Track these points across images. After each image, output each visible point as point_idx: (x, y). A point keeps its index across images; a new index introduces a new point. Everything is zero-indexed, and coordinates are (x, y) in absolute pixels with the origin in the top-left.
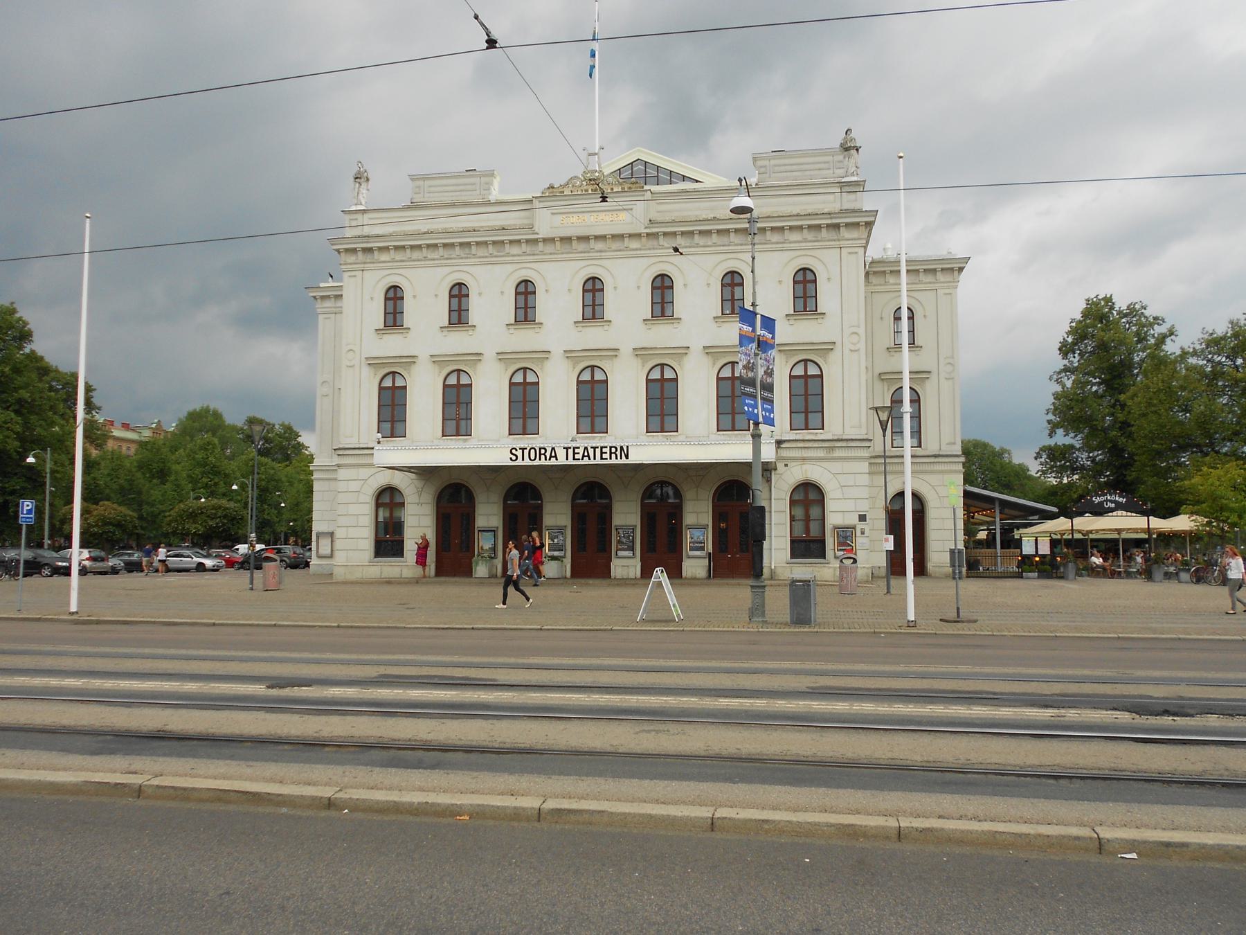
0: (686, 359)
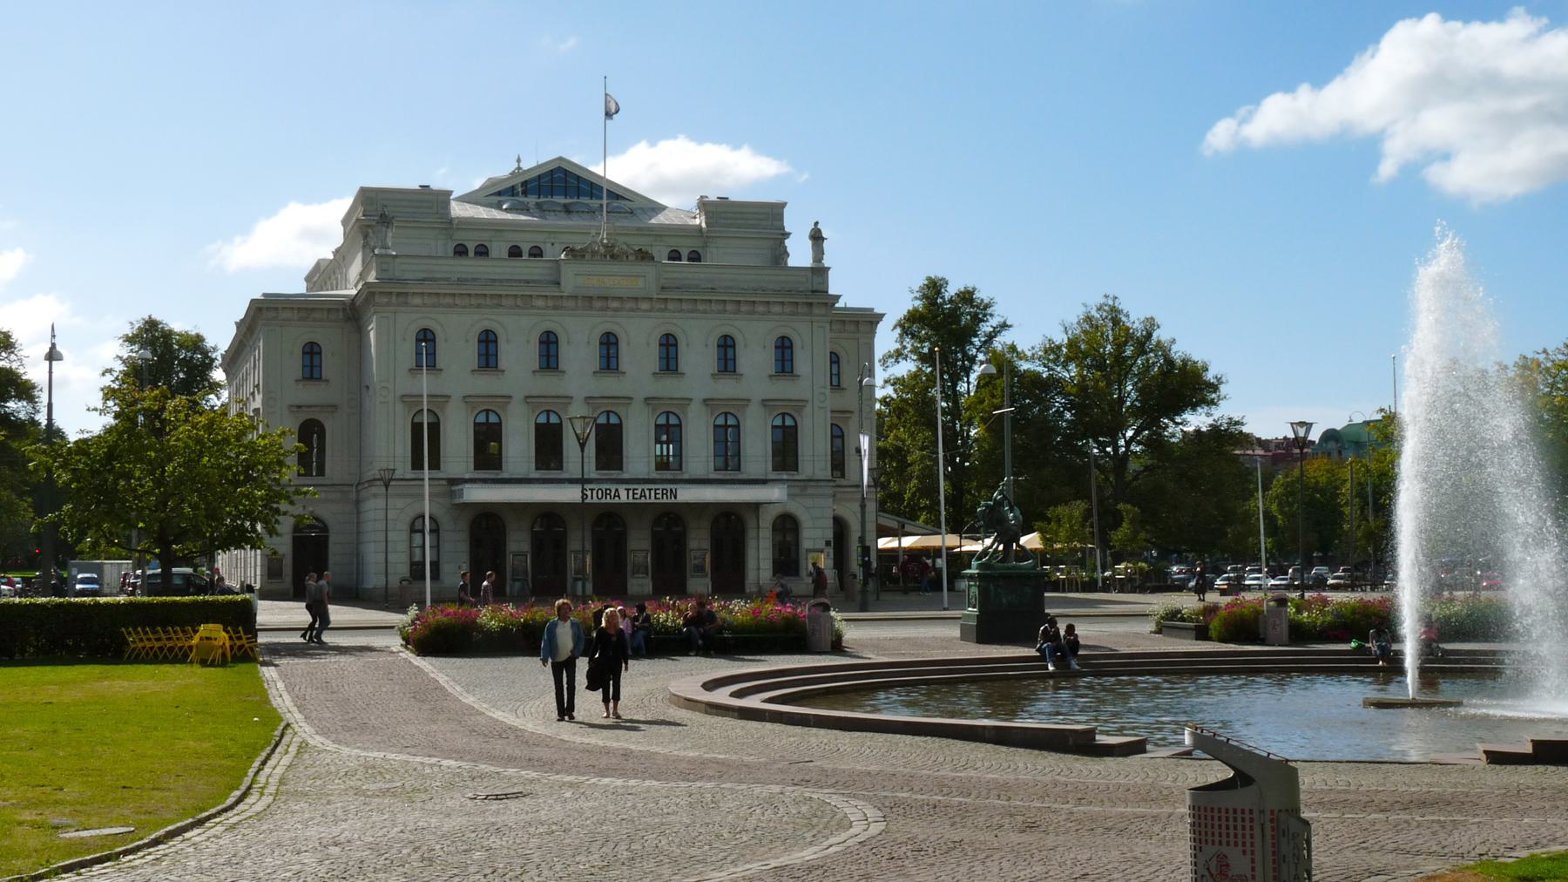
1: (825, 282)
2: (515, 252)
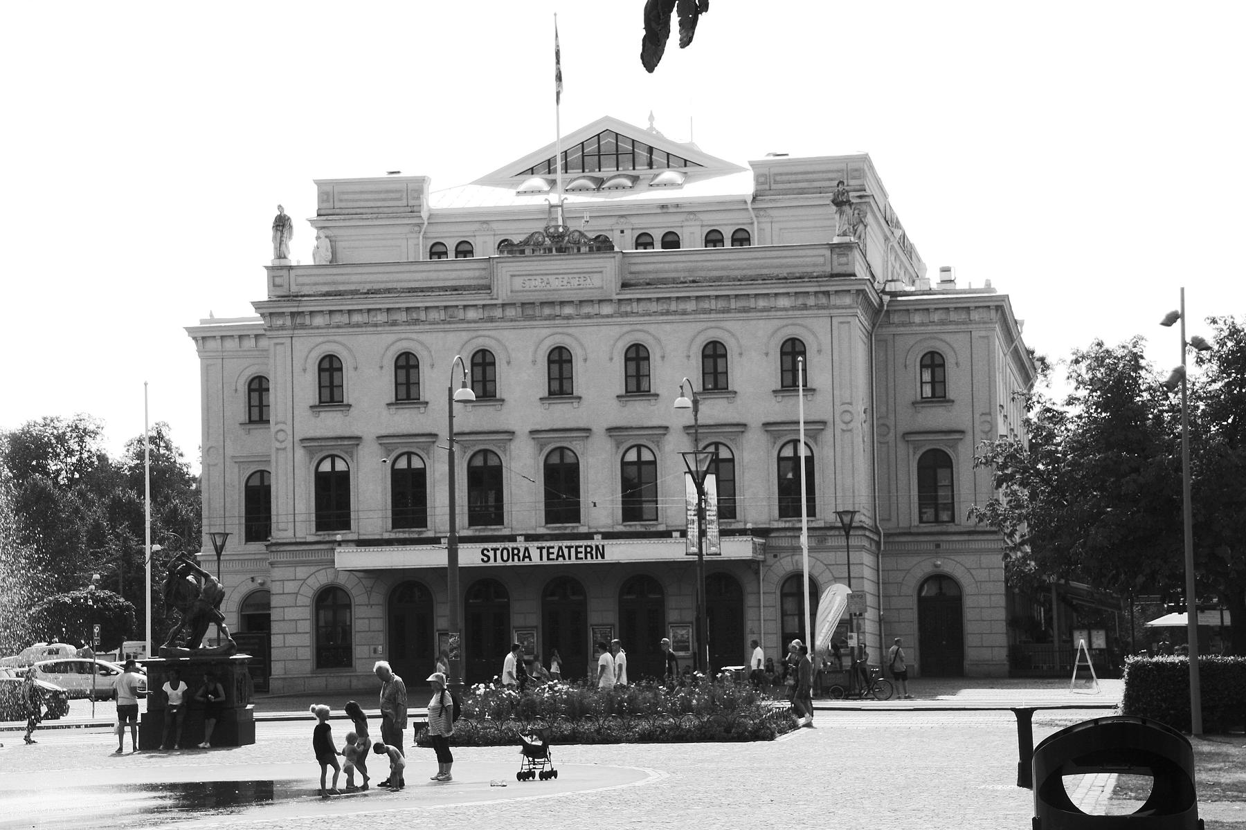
2: (714, 238)
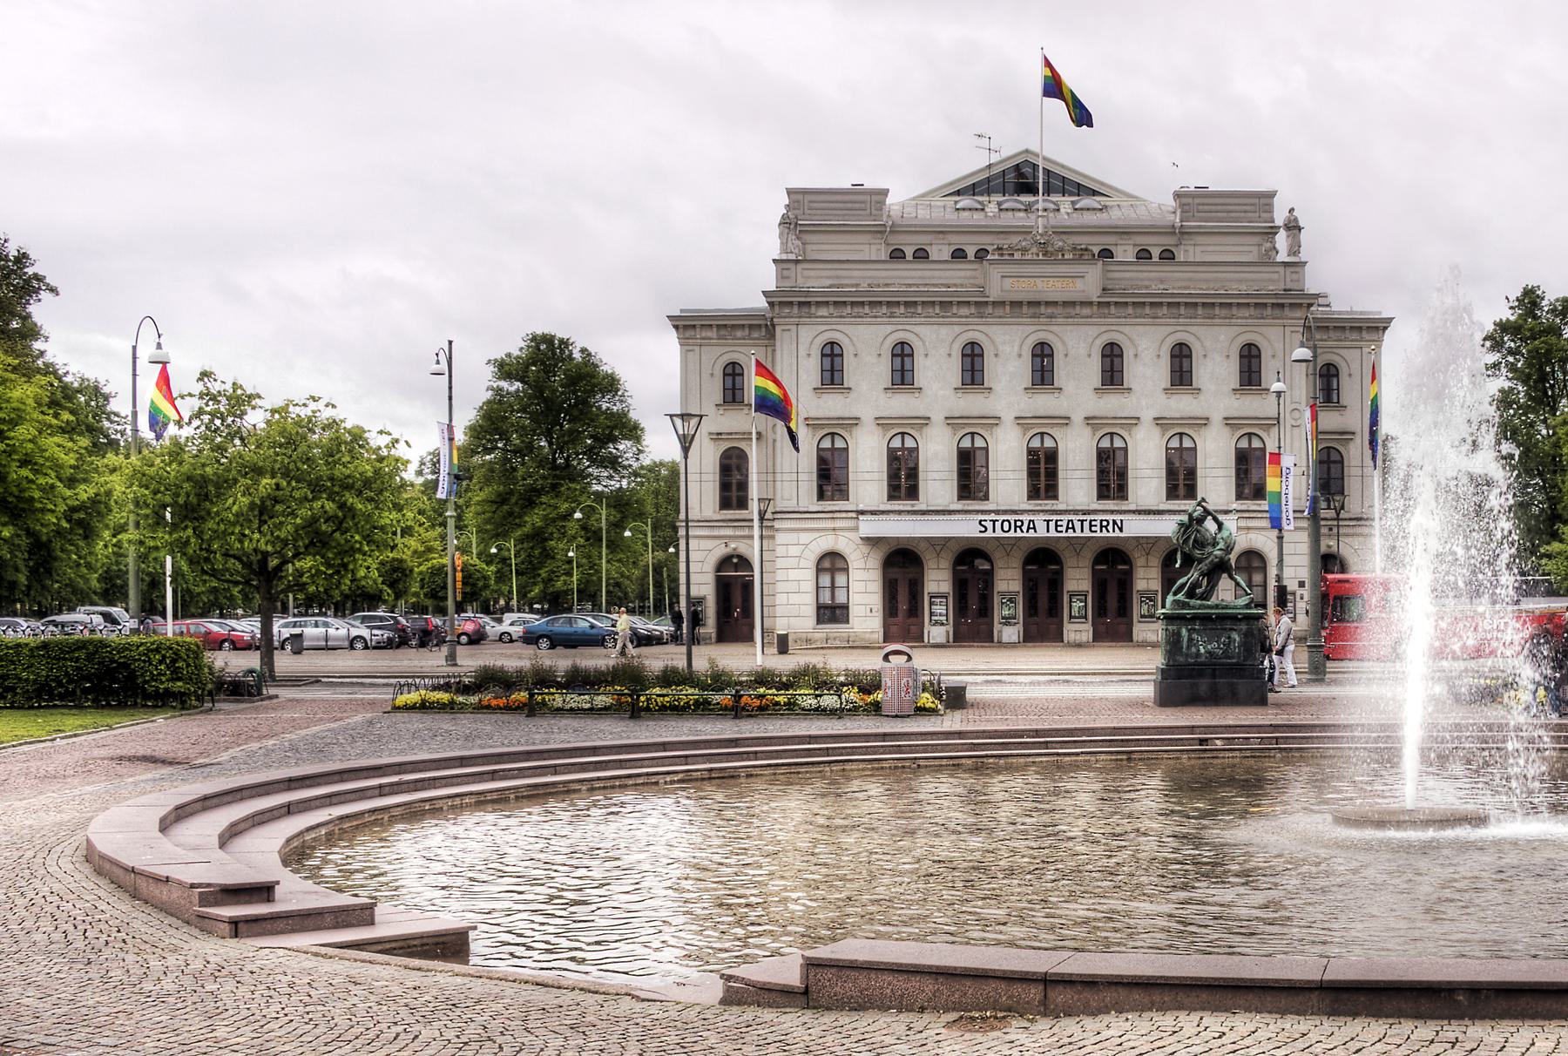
0: (1135, 430)
1: (1301, 280)
2: (959, 255)
